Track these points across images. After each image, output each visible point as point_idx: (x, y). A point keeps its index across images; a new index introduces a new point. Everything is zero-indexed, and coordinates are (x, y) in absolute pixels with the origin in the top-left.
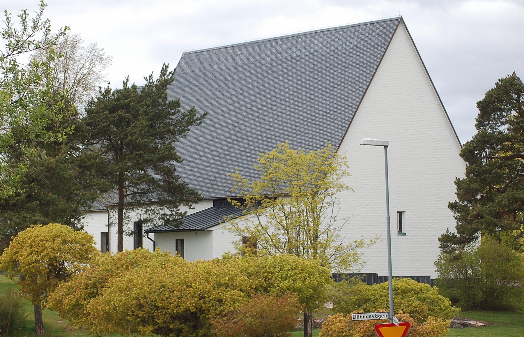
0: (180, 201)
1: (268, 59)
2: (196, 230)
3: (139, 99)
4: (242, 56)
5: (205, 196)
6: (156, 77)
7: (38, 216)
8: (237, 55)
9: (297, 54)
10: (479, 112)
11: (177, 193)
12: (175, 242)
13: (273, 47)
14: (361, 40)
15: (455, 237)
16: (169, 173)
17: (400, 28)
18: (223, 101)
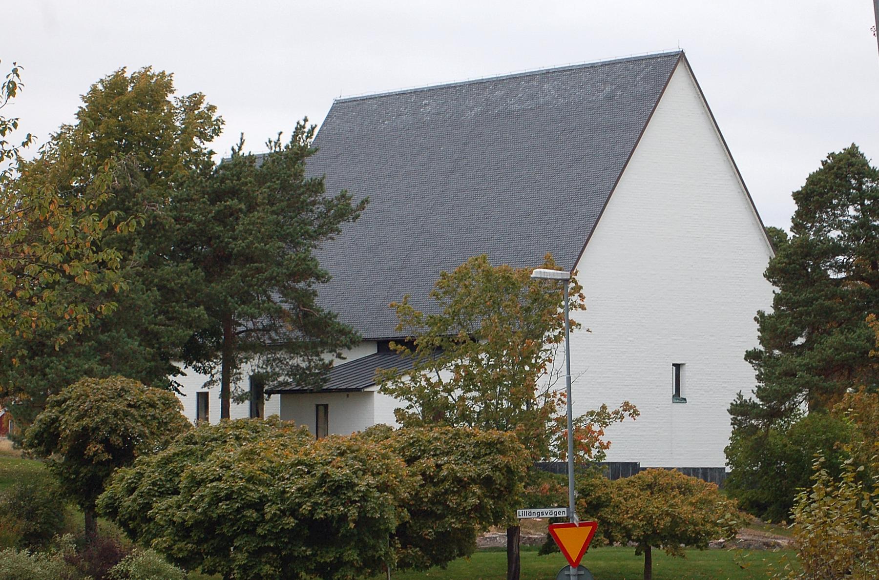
0: (323, 344)
1: (470, 114)
2: (347, 390)
3: (262, 179)
4: (429, 109)
5: (365, 335)
6: (286, 140)
7: (93, 364)
8: (421, 106)
9: (517, 107)
10: (796, 208)
11: (321, 331)
12: (314, 408)
13: (478, 94)
14: (619, 87)
15: (755, 405)
16: (304, 299)
17: (680, 70)
18: (397, 180)
